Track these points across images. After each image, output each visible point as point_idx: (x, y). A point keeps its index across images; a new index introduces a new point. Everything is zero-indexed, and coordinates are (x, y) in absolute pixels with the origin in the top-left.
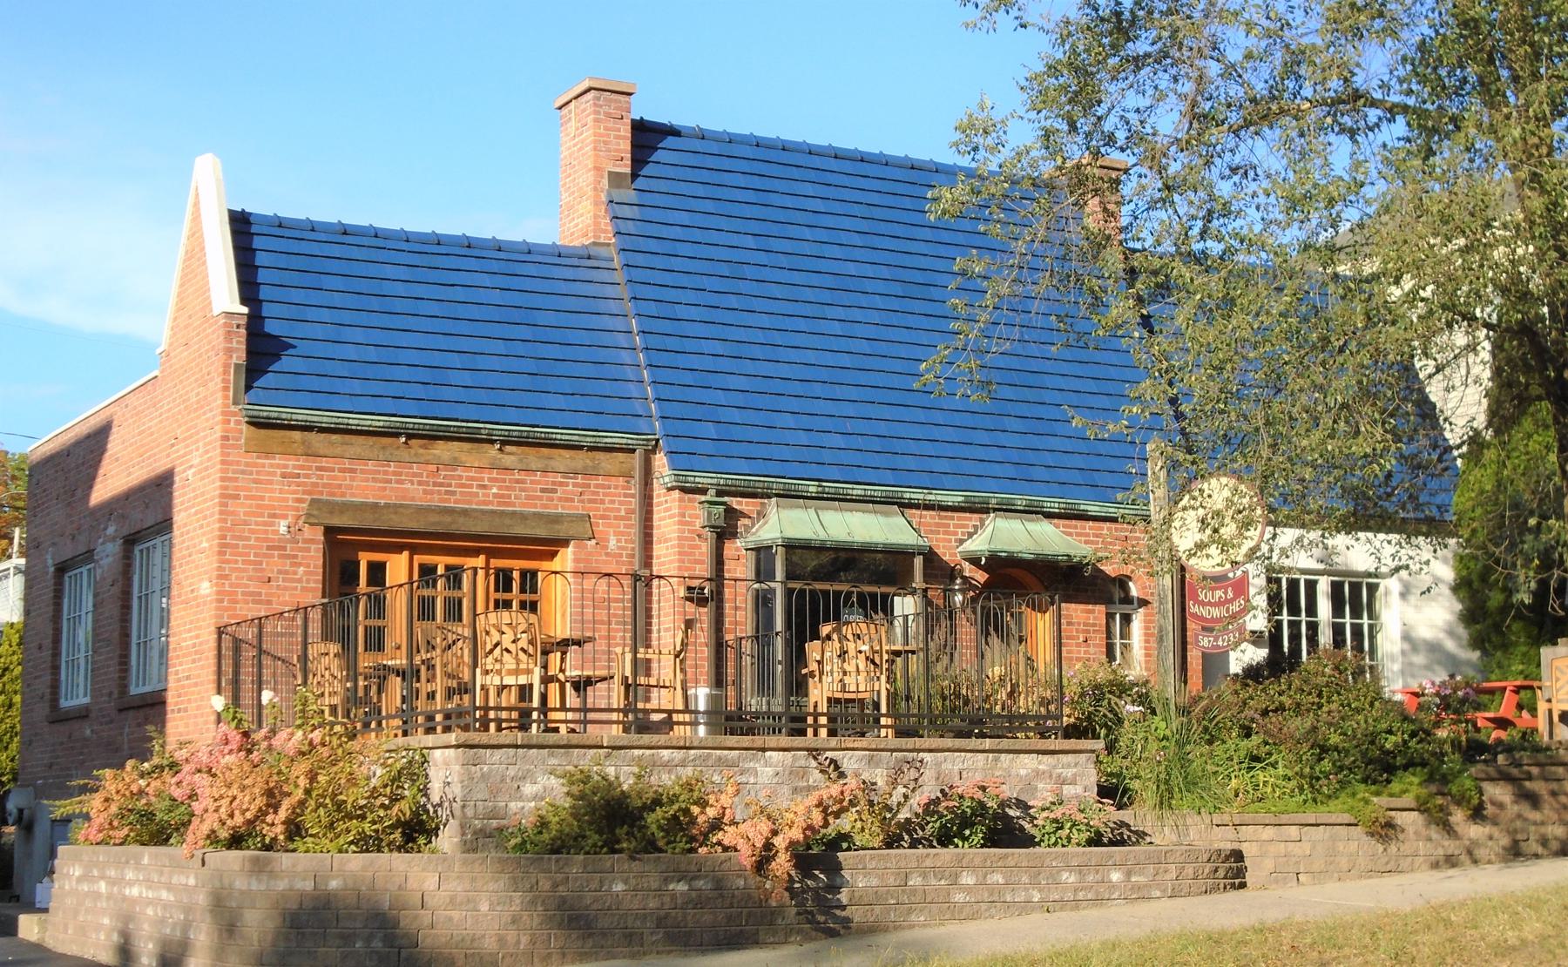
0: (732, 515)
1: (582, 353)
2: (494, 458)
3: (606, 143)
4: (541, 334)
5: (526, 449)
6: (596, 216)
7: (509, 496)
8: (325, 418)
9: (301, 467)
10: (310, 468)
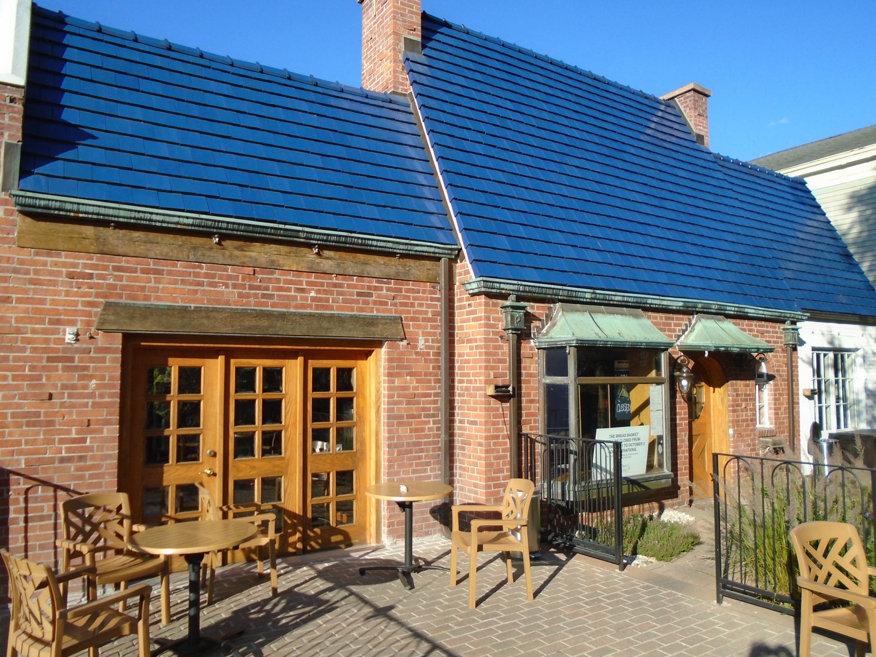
0: (529, 318)
1: (390, 173)
2: (313, 262)
3: (402, 15)
4: (353, 154)
5: (344, 255)
6: (395, 71)
7: (327, 300)
8: (123, 212)
9: (93, 266)
10: (106, 268)
